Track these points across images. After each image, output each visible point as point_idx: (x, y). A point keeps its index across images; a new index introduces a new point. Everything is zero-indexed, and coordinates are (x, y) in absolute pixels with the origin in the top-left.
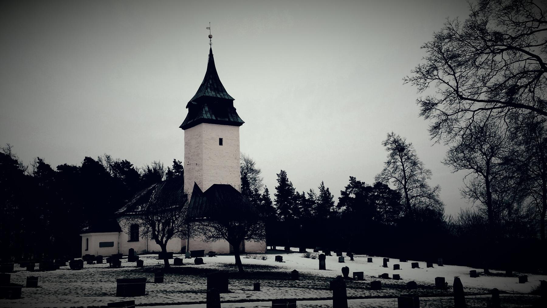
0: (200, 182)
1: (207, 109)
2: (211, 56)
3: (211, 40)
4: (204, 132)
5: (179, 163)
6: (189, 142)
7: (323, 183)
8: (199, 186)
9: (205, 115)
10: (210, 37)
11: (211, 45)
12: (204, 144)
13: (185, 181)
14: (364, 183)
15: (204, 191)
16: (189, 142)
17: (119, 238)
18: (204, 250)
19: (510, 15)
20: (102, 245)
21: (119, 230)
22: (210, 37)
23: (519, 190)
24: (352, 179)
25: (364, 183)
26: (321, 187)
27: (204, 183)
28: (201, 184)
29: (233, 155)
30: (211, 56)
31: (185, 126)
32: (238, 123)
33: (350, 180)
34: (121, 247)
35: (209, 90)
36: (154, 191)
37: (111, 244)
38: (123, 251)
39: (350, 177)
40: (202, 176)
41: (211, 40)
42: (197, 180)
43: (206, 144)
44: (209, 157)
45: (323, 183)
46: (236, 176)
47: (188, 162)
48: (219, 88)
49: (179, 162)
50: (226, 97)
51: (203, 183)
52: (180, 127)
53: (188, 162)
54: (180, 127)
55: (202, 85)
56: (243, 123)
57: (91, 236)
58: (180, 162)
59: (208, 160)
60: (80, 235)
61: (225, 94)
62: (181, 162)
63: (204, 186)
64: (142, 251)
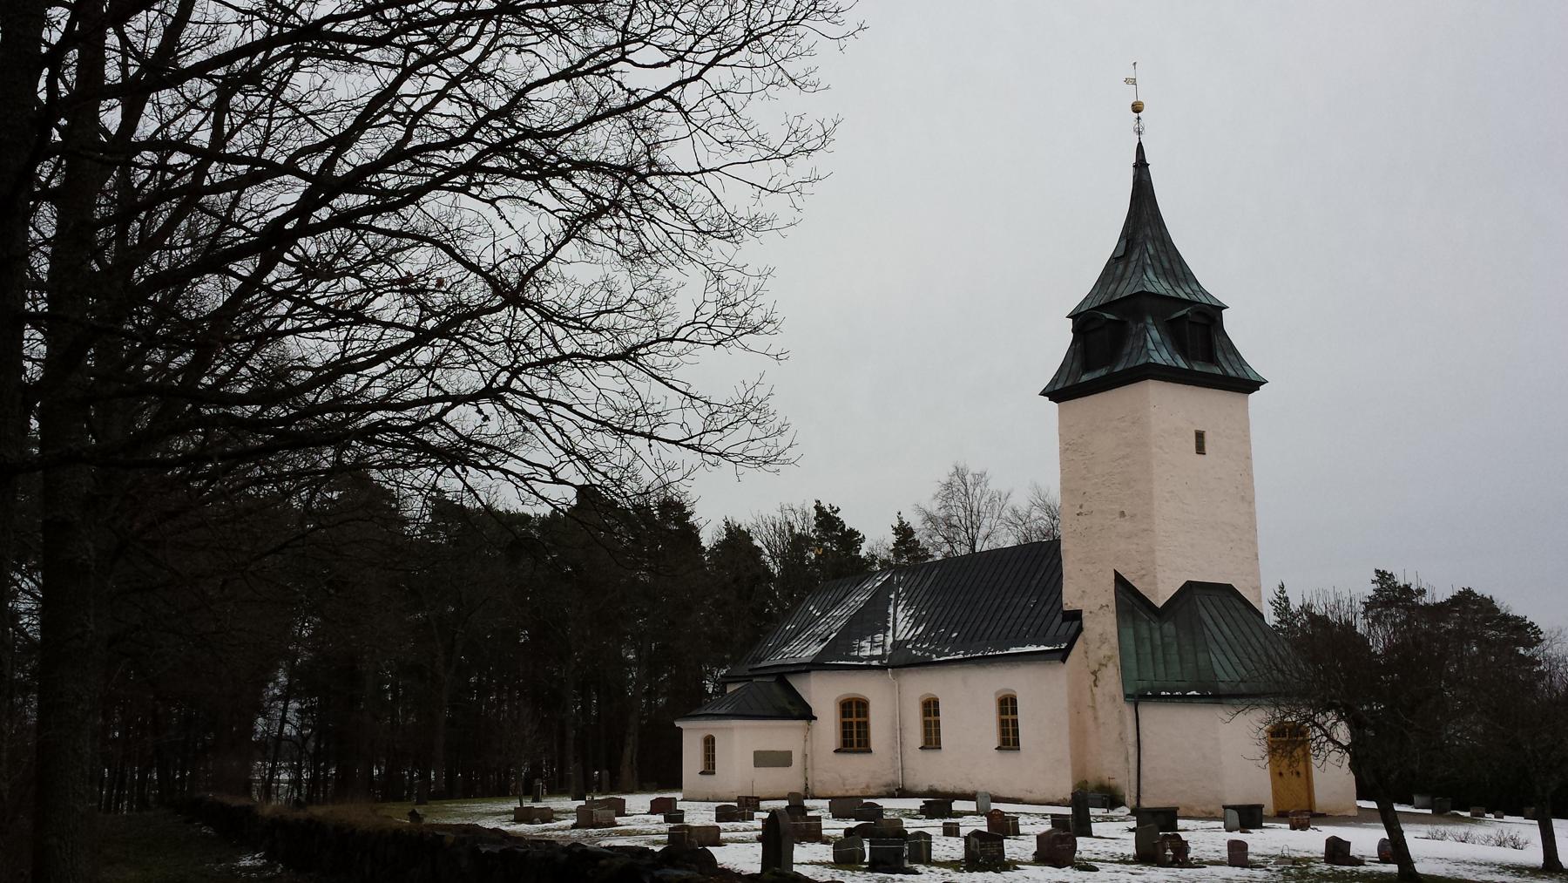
0: (1143, 572)
1: (1155, 334)
2: (1141, 166)
3: (1139, 118)
4: (1152, 409)
5: (833, 512)
6: (1080, 441)
7: (1282, 587)
8: (1139, 586)
9: (1156, 353)
10: (1137, 108)
11: (1139, 133)
12: (1154, 450)
13: (1067, 567)
14: (1424, 591)
15: (1160, 604)
16: (1080, 441)
17: (806, 741)
18: (1178, 808)
19: (554, 242)
20: (764, 759)
21: (805, 713)
22: (1137, 108)
23: (1491, 622)
24: (1382, 576)
25: (1422, 592)
26: (1277, 600)
27: (1158, 576)
28: (1146, 579)
29: (1237, 488)
30: (1141, 166)
31: (1056, 393)
32: (1248, 384)
33: (1373, 582)
34: (813, 769)
35: (1151, 274)
36: (892, 596)
37: (783, 759)
38: (820, 781)
39: (1377, 571)
40: (1153, 551)
41: (1139, 118)
42: (1127, 564)
43: (1161, 447)
44: (1172, 492)
45: (1282, 587)
46: (1247, 558)
47: (1081, 507)
48: (1176, 267)
49: (831, 508)
50: (1204, 300)
51: (1155, 577)
52: (1043, 393)
53: (1081, 507)
54: (1043, 393)
55: (1114, 260)
56: (1263, 383)
57: (731, 729)
58: (836, 509)
59: (1167, 501)
60: (678, 724)
61: (1195, 287)
62: (838, 510)
63: (1160, 586)
64: (885, 786)
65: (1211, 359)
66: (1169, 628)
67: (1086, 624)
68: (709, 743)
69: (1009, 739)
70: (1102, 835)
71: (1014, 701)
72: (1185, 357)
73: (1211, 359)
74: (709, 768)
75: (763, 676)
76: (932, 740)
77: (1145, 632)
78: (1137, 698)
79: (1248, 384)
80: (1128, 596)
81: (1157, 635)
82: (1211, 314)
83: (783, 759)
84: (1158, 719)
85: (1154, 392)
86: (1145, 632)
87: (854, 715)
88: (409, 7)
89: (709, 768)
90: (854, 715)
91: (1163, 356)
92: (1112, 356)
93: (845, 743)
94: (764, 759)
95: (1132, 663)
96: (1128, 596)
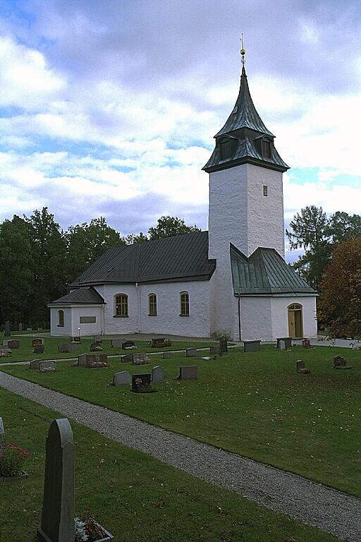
20: (83, 320)
21: (101, 301)
31: (208, 169)
37: (92, 320)
55: (233, 115)
65: (270, 157)
66: (252, 266)
67: (218, 265)
68: (61, 313)
69: (185, 311)
70: (116, 172)
71: (187, 296)
72: (261, 155)
73: (270, 157)
74: (61, 324)
75: (84, 286)
76: (153, 312)
77: (242, 267)
78: (238, 296)
79: (283, 168)
80: (236, 254)
81: (247, 269)
82: (271, 139)
83: (92, 320)
84: (245, 303)
85: (249, 169)
86: (242, 267)
87: (121, 300)
88: (279, 328)
89: (61, 324)
90: (121, 300)
91: (253, 155)
92: (233, 154)
93: (117, 313)
94: (83, 320)
95: (237, 280)
96: (236, 254)
